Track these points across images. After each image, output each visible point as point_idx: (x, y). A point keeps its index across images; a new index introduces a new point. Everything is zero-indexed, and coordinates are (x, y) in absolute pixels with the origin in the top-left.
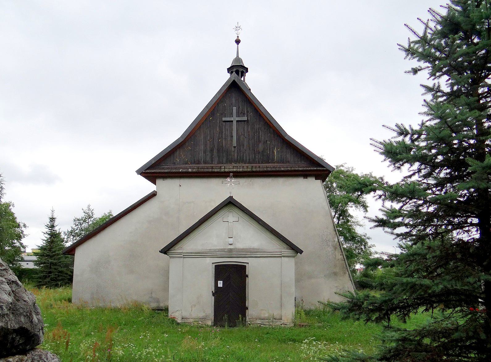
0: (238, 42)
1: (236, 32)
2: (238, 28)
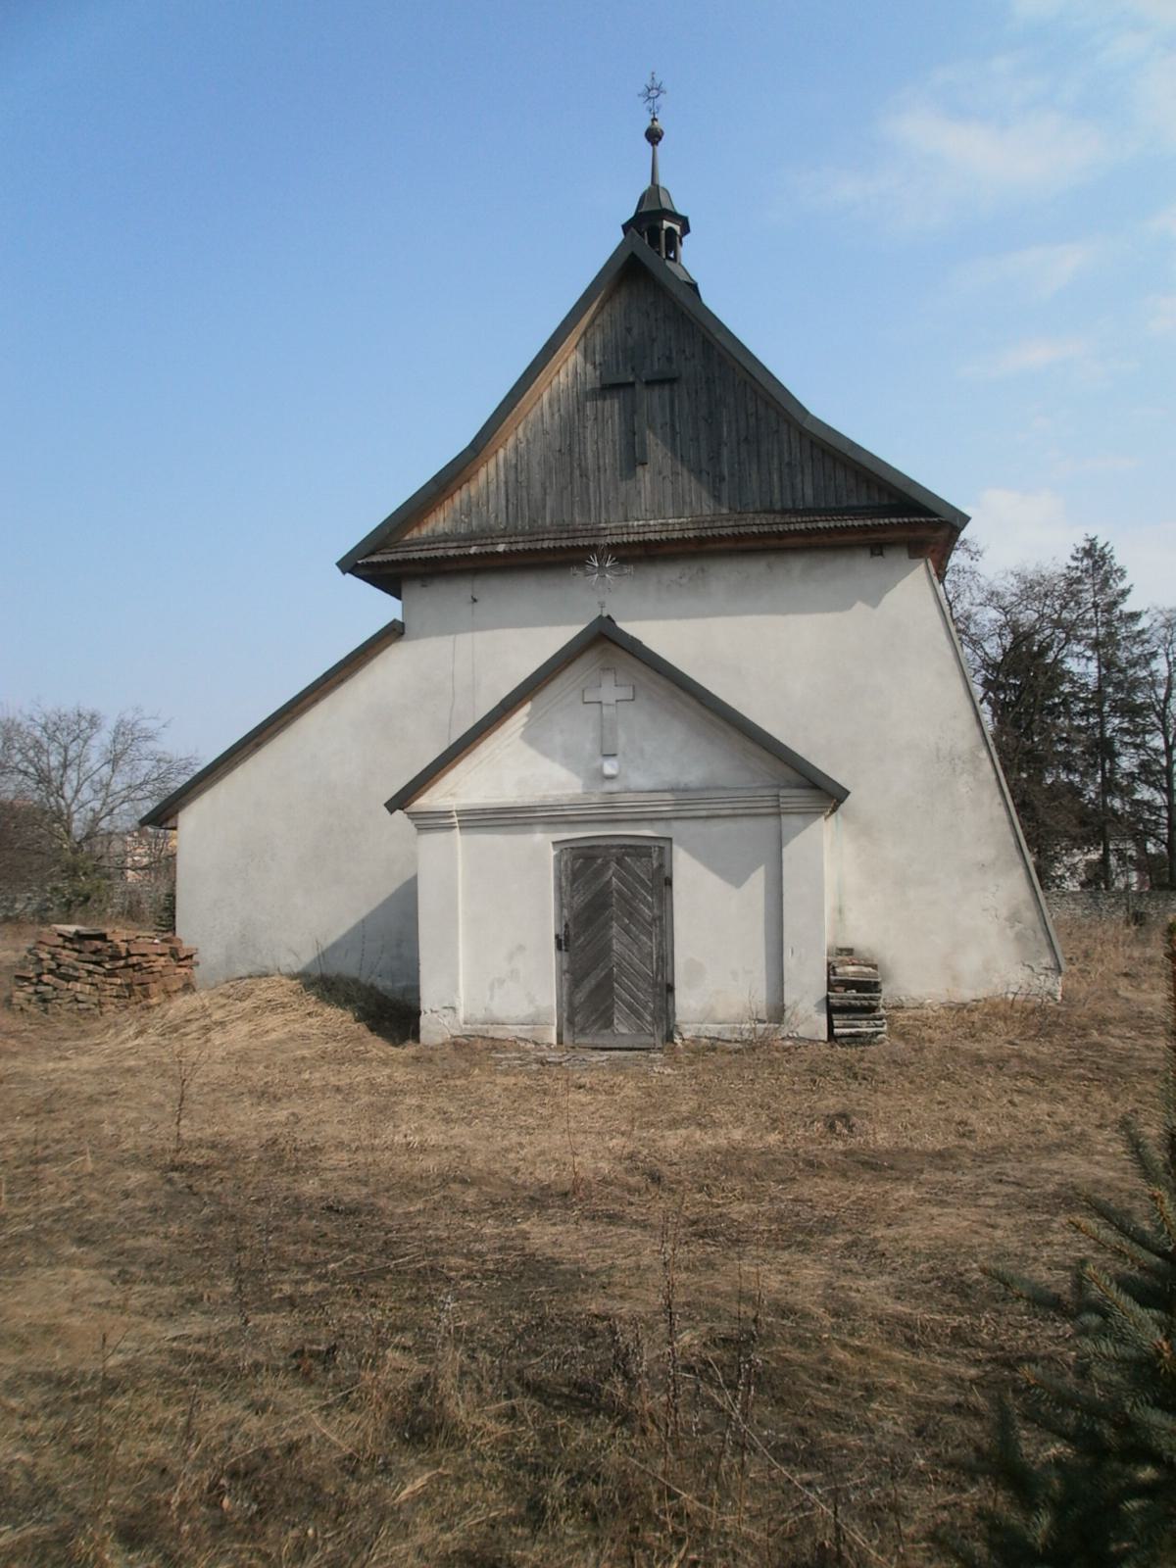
0: (654, 136)
1: (649, 104)
2: (652, 92)
